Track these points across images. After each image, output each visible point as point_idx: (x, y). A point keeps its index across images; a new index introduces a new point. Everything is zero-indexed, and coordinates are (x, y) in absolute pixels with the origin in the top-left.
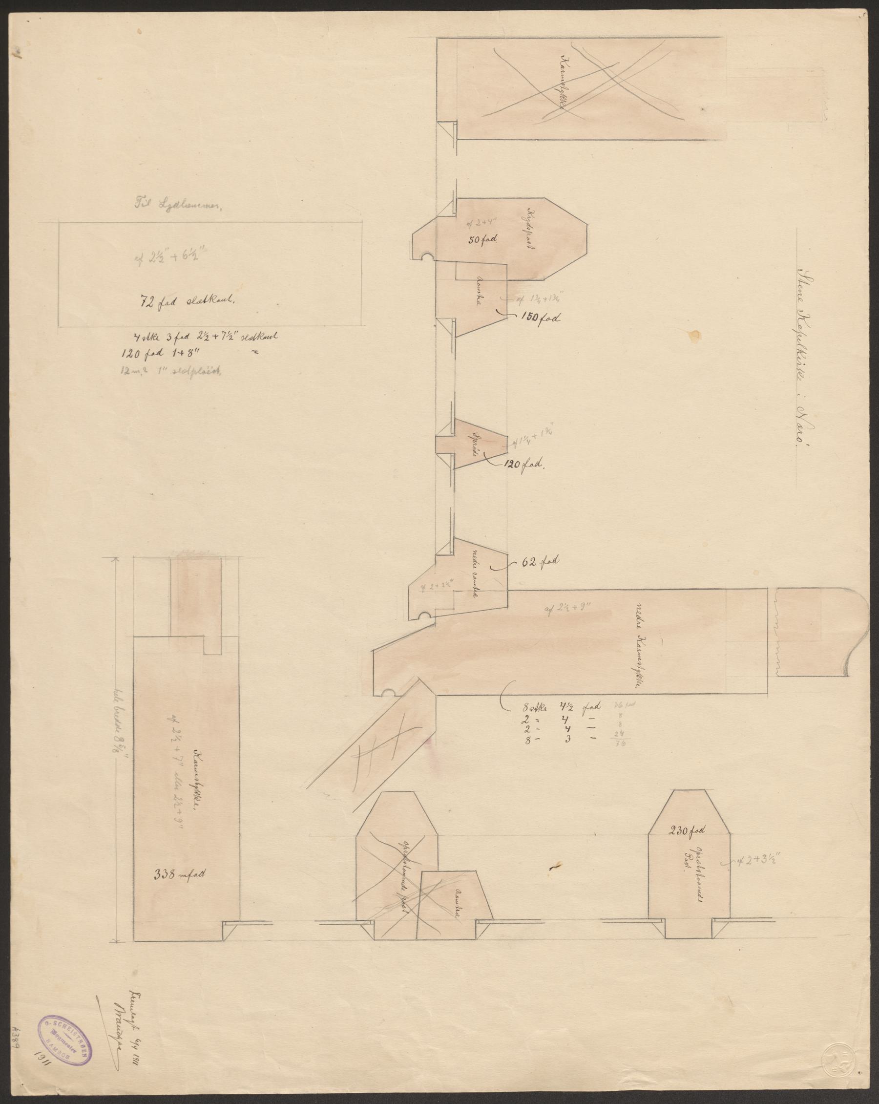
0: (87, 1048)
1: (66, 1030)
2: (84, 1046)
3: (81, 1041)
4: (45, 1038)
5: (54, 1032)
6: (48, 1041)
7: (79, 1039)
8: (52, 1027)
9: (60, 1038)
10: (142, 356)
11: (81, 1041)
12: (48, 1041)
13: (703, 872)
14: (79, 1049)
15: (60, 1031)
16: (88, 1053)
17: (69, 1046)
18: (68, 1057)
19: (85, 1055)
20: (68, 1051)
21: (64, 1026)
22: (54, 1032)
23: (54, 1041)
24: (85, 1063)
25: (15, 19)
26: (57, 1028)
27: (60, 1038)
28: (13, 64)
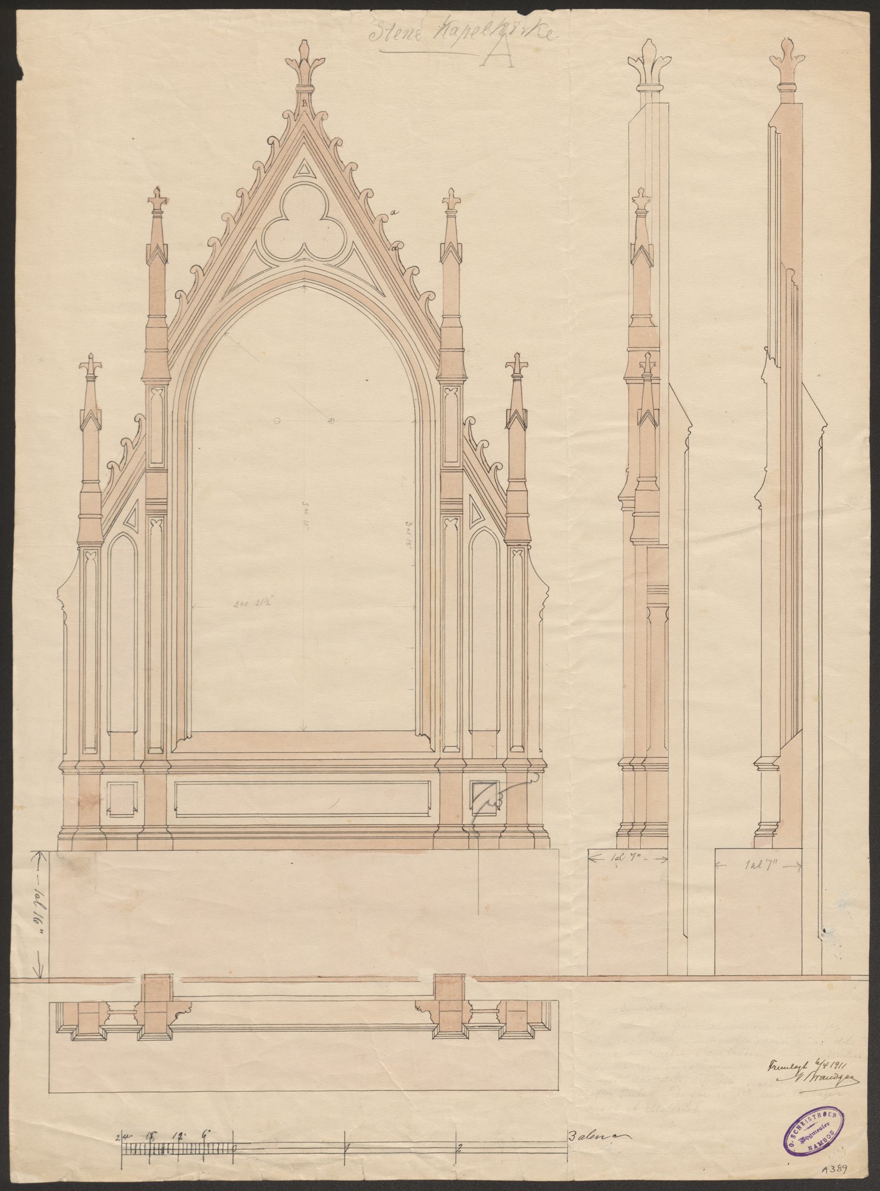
0: (827, 1111)
1: (803, 1128)
2: (825, 1114)
3: (819, 1115)
4: (806, 1150)
5: (803, 1140)
6: (810, 1148)
7: (816, 1116)
8: (796, 1141)
9: (810, 1136)
10: (765, 865)
11: (819, 1115)
12: (810, 1148)
13: (194, 1136)
14: (823, 1120)
15: (803, 1133)
16: (833, 1111)
17: (821, 1129)
18: (831, 1132)
19: (835, 1115)
20: (826, 1131)
21: (799, 1128)
22: (803, 1140)
23: (808, 1143)
24: (843, 1115)
25: (22, 15)
26: (799, 1136)
27: (810, 1136)
28: (27, 95)
